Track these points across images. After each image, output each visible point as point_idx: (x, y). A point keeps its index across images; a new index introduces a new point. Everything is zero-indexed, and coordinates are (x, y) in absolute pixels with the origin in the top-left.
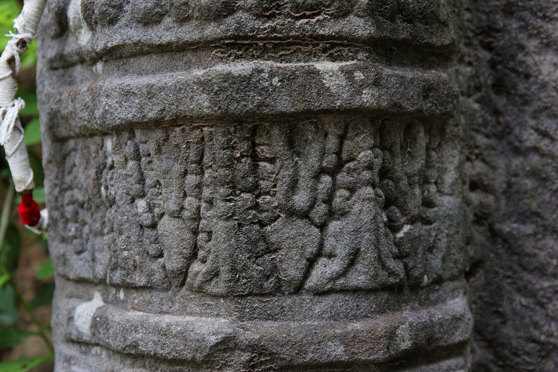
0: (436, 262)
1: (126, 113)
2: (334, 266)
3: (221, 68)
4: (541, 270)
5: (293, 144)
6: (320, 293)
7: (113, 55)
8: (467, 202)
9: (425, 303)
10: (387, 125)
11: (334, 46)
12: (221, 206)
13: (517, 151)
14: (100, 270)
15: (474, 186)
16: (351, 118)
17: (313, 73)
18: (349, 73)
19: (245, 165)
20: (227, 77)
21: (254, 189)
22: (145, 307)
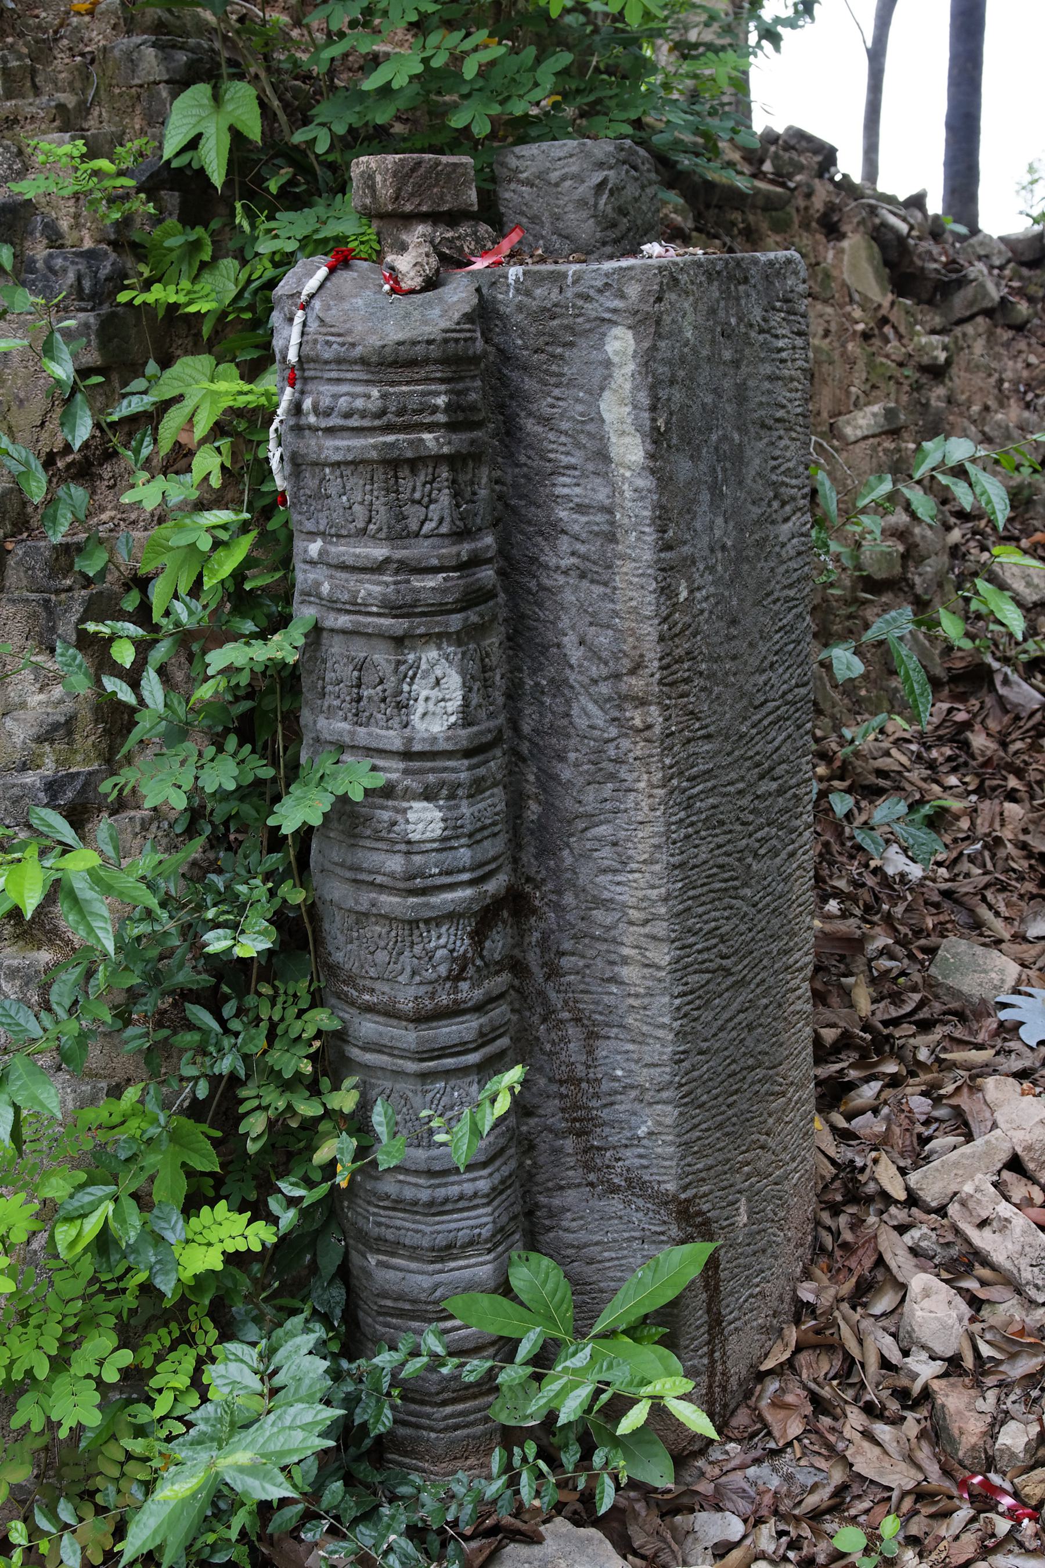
0: (478, 521)
1: (338, 457)
2: (433, 524)
3: (381, 439)
4: (529, 523)
5: (414, 472)
6: (427, 537)
7: (330, 431)
8: (493, 491)
9: (473, 540)
10: (454, 461)
11: (430, 427)
12: (383, 500)
13: (518, 465)
14: (322, 528)
15: (497, 482)
16: (438, 459)
17: (422, 440)
18: (437, 439)
19: (392, 481)
20: (385, 443)
21: (397, 492)
22: (347, 545)
